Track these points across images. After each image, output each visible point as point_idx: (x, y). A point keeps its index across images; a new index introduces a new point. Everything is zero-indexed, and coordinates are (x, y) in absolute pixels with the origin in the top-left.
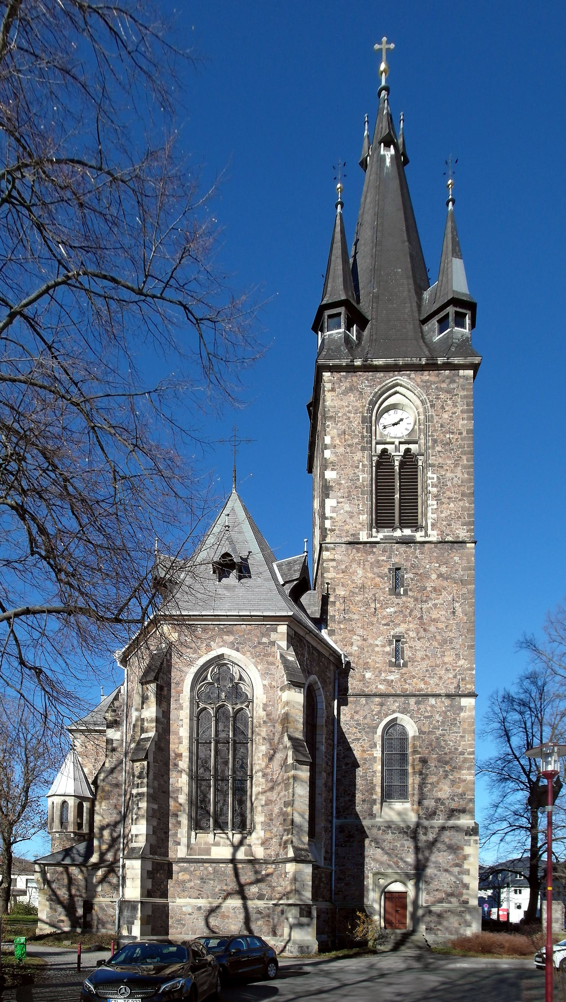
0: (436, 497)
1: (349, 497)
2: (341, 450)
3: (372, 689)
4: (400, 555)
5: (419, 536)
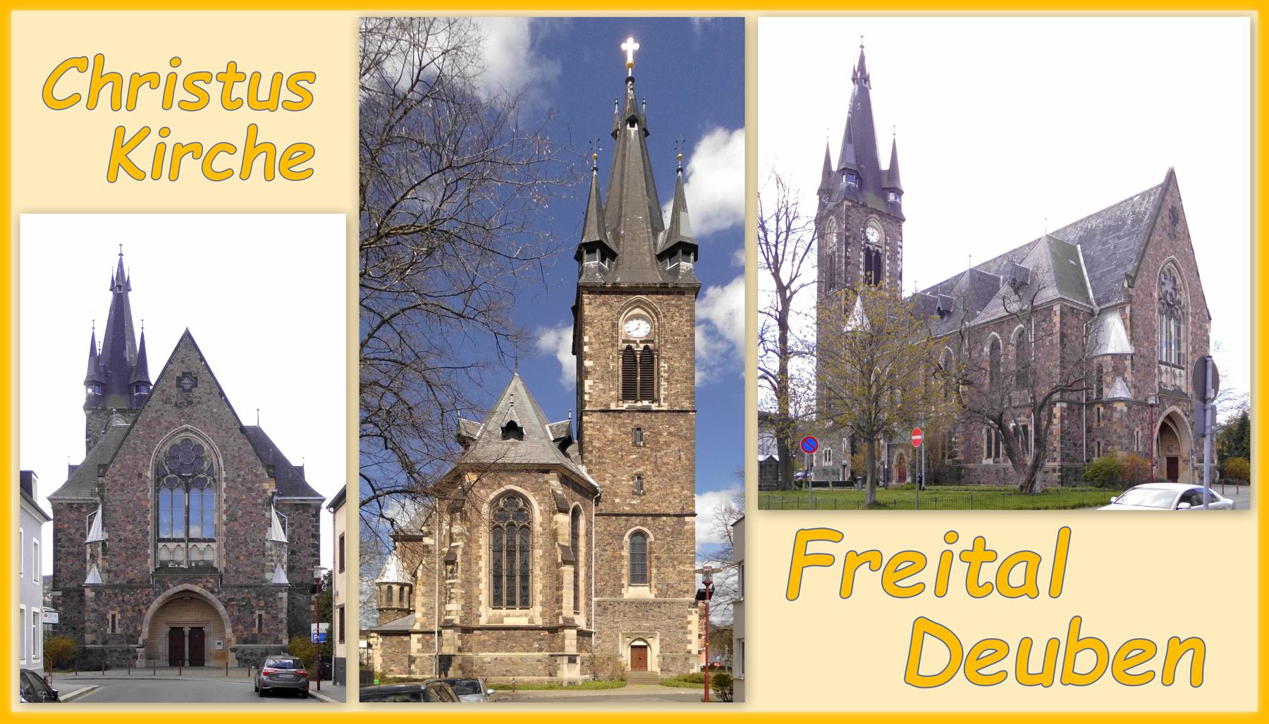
0: (667, 380)
1: (602, 379)
2: (596, 346)
3: (620, 510)
4: (639, 420)
5: (654, 407)
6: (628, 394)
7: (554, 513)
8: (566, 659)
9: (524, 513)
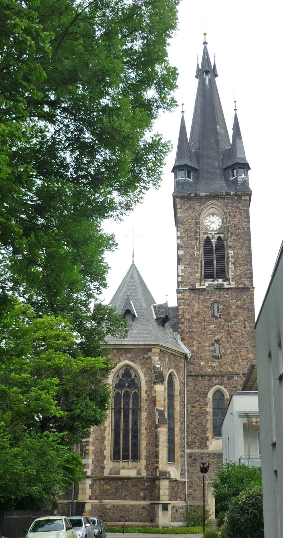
0: (233, 263)
1: (190, 264)
2: (185, 239)
6: (208, 275)
7: (154, 383)
8: (161, 507)
9: (134, 384)
